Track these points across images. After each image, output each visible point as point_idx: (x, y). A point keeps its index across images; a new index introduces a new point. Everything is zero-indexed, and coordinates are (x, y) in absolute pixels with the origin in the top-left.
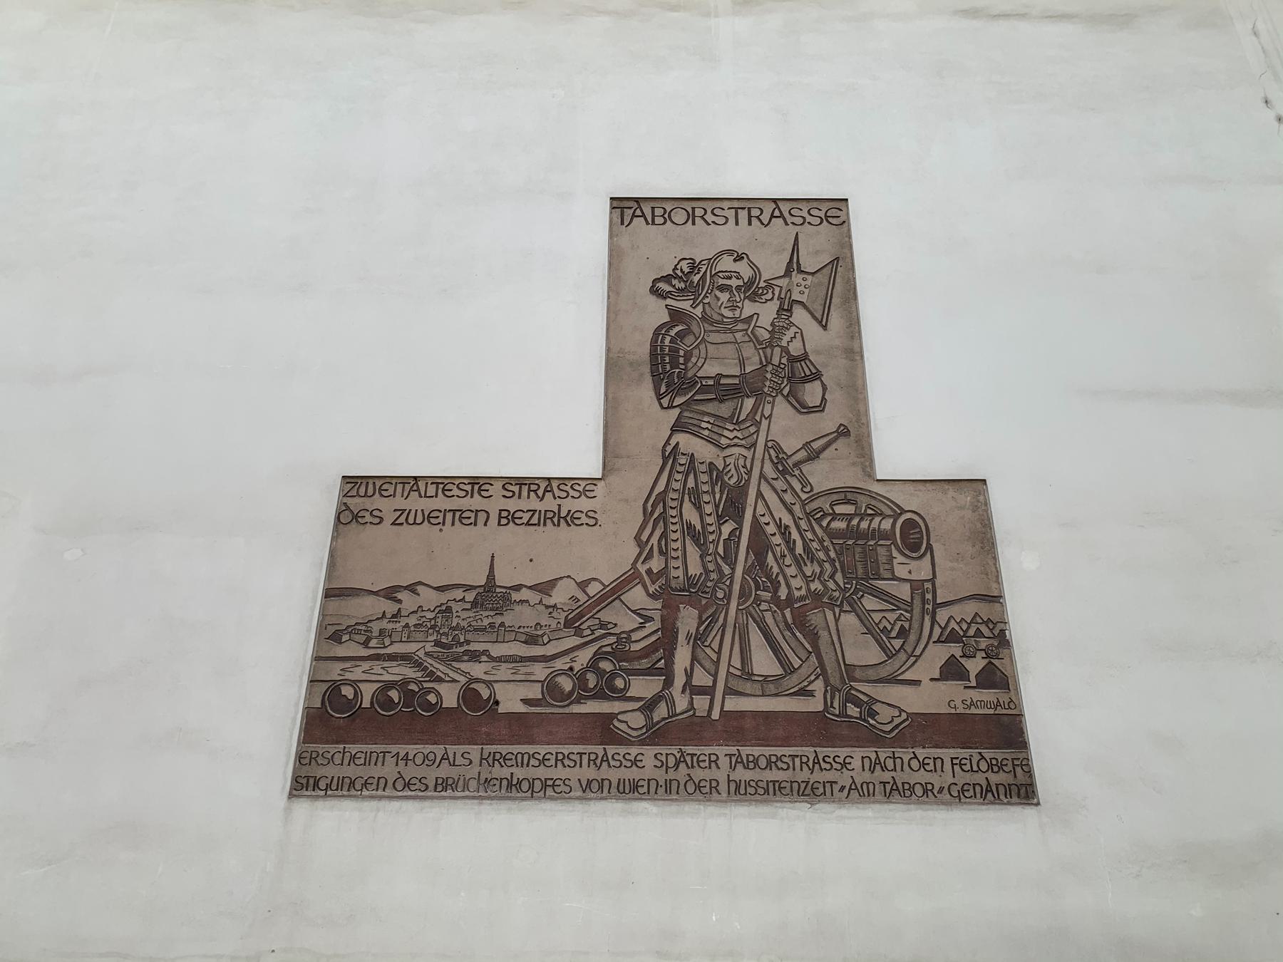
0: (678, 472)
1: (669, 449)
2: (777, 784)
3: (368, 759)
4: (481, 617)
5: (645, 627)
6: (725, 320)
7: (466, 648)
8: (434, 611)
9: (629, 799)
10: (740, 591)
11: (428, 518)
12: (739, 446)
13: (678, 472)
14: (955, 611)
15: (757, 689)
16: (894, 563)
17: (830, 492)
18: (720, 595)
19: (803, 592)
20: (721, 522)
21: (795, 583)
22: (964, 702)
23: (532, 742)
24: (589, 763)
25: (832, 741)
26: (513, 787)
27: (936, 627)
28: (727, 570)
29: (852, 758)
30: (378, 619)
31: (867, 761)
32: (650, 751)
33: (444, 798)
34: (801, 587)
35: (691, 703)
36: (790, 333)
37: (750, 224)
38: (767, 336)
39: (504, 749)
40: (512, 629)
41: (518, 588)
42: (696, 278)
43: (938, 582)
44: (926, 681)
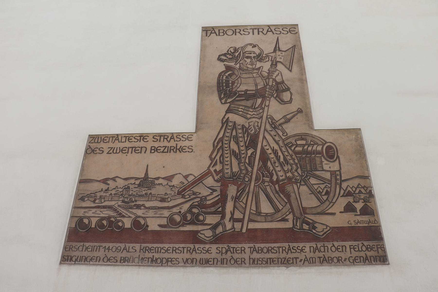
0: (228, 129)
1: (225, 120)
2: (271, 260)
3: (93, 249)
4: (142, 190)
5: (213, 194)
6: (249, 69)
7: (135, 203)
8: (122, 188)
9: (205, 267)
10: (256, 177)
11: (122, 151)
12: (255, 118)
13: (228, 129)
14: (350, 183)
15: (263, 219)
16: (323, 164)
17: (295, 135)
18: (247, 179)
19: (284, 177)
20: (247, 149)
21: (280, 174)
22: (355, 221)
23: (162, 242)
24: (187, 252)
25: (296, 240)
26: (154, 262)
27: (342, 190)
28: (250, 169)
29: (305, 247)
30: (99, 191)
31: (312, 248)
32: (214, 246)
33: (124, 265)
34: (283, 175)
35: (233, 225)
36: (276, 73)
37: (259, 34)
38: (266, 74)
39: (150, 245)
40: (155, 195)
41: (158, 178)
42: (237, 54)
43: (342, 171)
44: (338, 213)
